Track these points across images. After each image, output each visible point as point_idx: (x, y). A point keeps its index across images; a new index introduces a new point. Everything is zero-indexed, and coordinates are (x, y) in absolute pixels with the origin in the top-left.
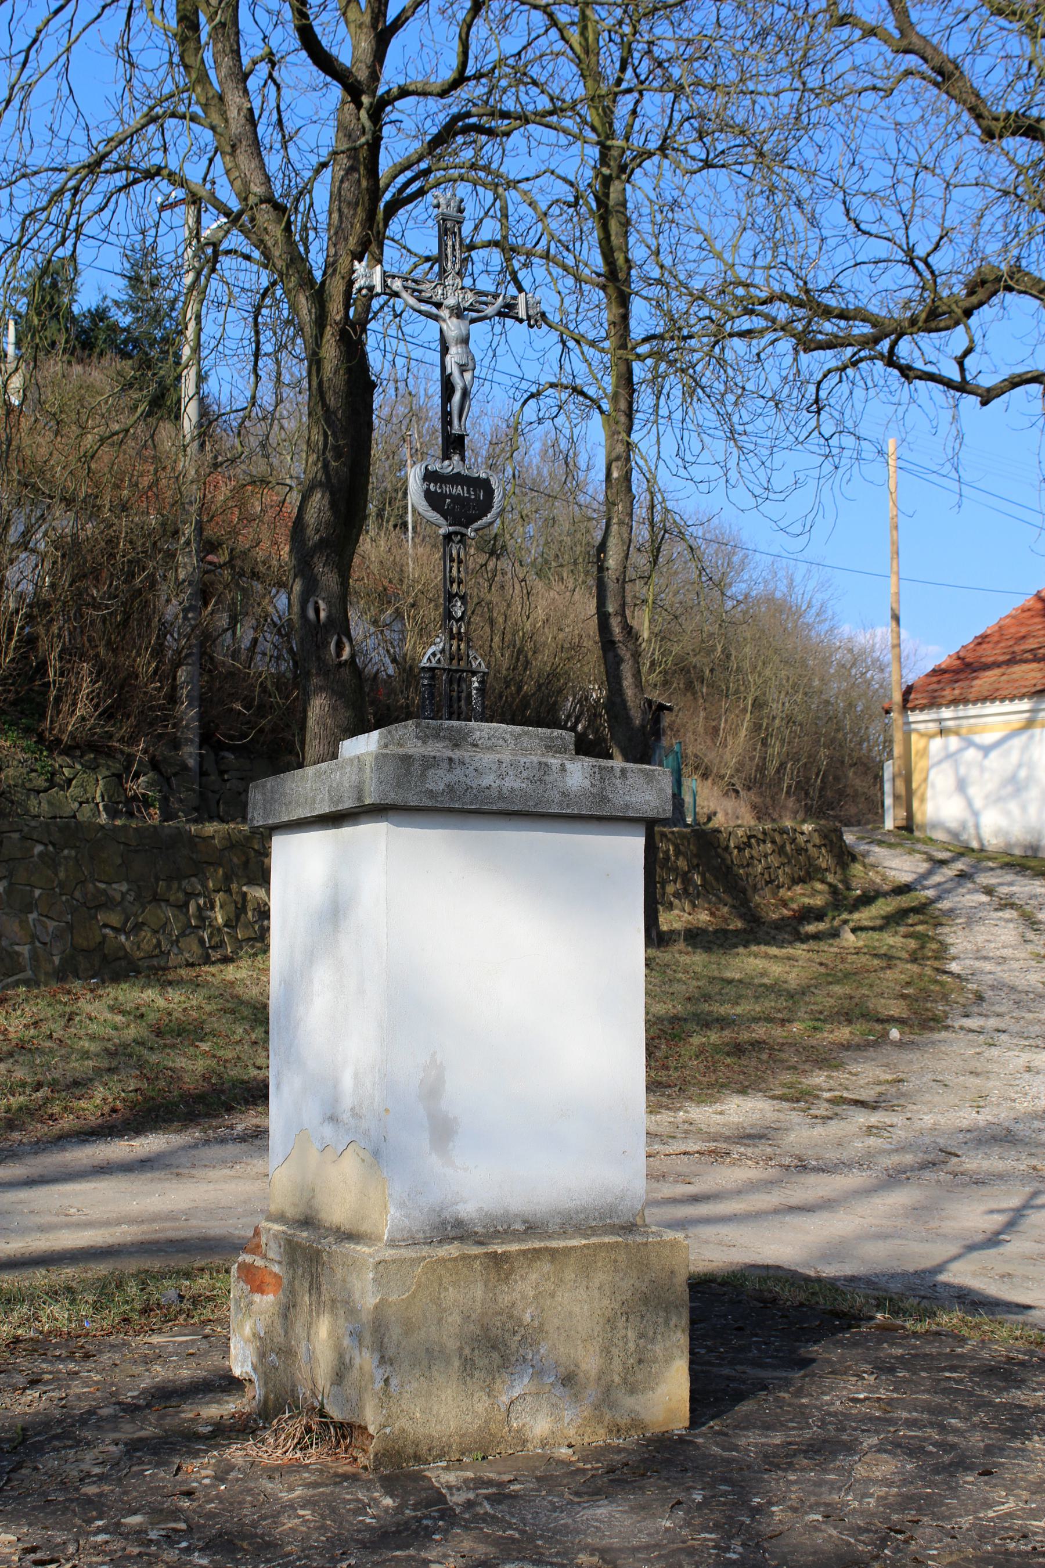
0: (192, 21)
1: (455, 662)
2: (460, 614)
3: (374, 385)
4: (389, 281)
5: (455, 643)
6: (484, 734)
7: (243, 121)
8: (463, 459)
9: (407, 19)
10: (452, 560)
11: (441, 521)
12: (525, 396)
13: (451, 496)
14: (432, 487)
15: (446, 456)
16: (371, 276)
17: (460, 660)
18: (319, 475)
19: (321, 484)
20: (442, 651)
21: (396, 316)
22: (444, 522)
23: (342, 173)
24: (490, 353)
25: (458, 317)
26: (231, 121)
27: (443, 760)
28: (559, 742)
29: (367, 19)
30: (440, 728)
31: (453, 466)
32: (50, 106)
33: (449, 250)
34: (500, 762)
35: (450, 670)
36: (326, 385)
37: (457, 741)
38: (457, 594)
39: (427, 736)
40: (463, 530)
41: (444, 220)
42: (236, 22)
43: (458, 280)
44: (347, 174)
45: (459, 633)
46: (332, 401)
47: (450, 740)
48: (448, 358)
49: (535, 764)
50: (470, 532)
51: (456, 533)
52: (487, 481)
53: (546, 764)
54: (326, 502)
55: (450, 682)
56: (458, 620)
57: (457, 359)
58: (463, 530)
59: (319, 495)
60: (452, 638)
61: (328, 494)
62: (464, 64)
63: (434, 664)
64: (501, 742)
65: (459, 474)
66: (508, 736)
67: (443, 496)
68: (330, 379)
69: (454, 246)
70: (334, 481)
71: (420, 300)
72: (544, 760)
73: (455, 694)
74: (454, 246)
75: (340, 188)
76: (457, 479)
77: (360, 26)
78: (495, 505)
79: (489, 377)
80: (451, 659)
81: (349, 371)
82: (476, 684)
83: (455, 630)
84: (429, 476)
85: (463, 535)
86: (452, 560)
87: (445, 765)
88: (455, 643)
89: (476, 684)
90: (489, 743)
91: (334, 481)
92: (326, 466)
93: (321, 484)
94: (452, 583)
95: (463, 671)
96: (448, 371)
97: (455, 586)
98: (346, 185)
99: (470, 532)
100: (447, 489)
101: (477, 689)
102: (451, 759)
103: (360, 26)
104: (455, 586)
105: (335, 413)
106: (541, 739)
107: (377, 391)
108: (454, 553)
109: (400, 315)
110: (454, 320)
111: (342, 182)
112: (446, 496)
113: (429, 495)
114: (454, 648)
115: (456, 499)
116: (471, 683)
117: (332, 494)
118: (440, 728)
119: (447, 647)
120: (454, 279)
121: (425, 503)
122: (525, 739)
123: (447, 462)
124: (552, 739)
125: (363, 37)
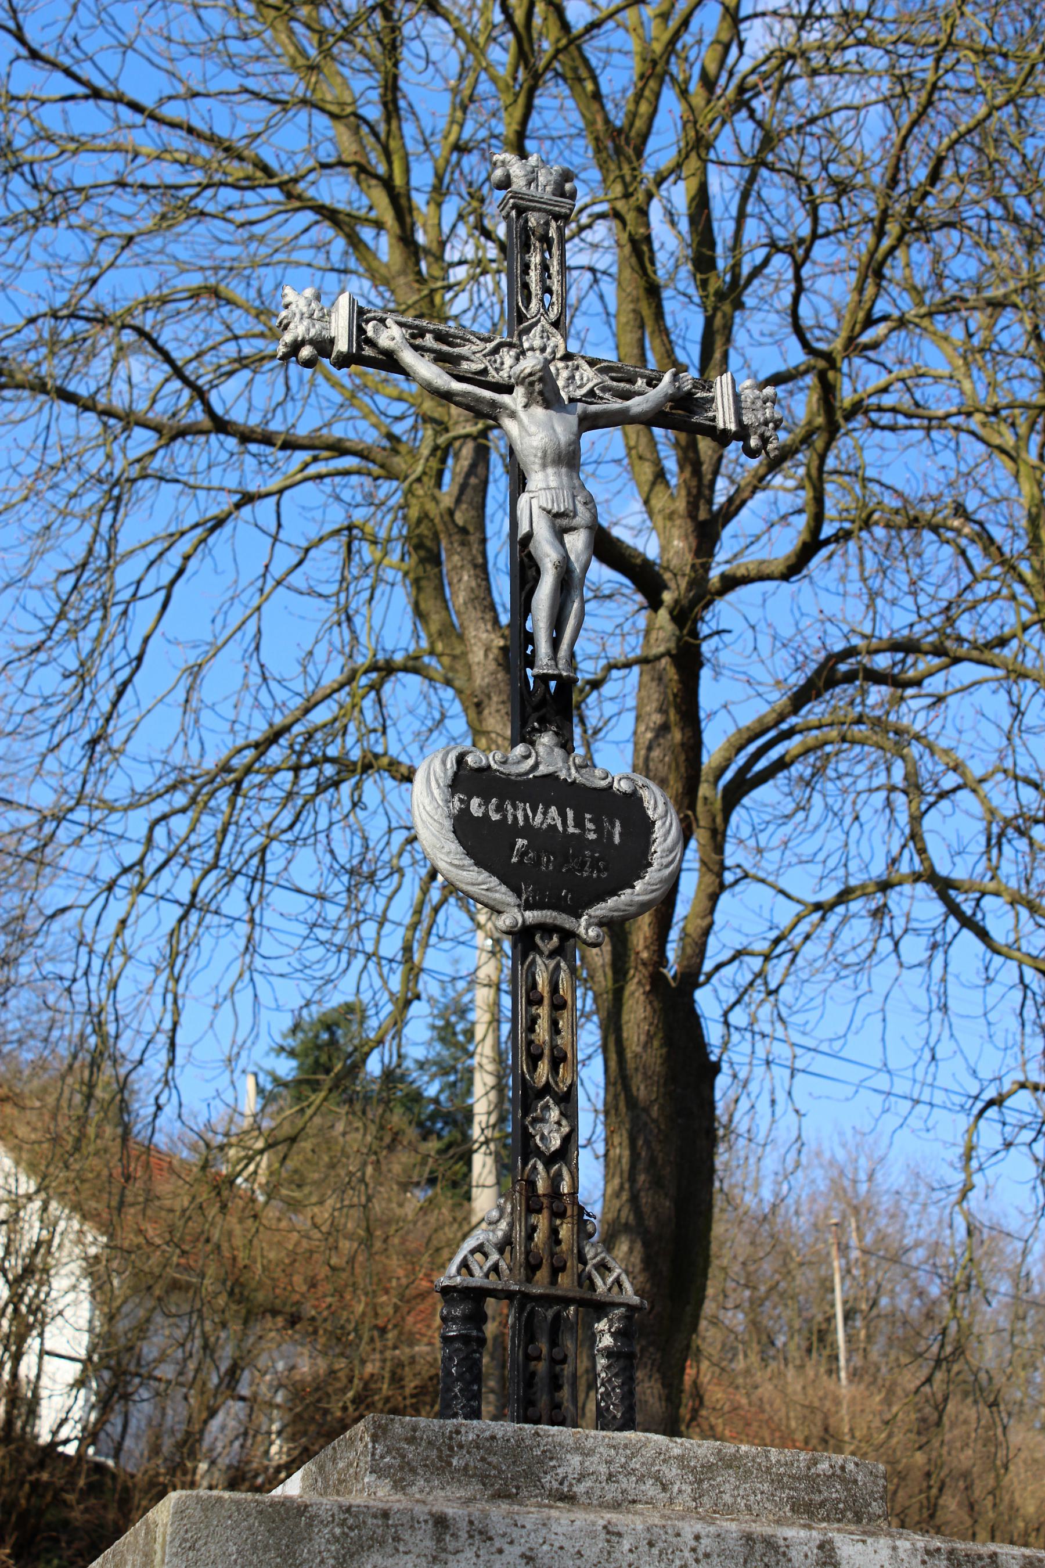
0: (429, 550)
1: (542, 1275)
2: (556, 1143)
3: (715, 1069)
4: (370, 328)
5: (542, 1221)
6: (594, 1463)
7: (492, 666)
8: (567, 746)
9: (743, 503)
10: (534, 1001)
11: (503, 894)
12: (980, 1105)
13: (527, 831)
14: (476, 807)
15: (523, 735)
16: (325, 317)
17: (556, 1271)
18: (624, 1214)
19: (627, 1228)
20: (505, 1245)
21: (770, 993)
22: (511, 898)
23: (649, 735)
24: (927, 1055)
25: (547, 405)
26: (475, 668)
27: (413, 1523)
28: (836, 1492)
29: (681, 505)
30: (451, 1444)
31: (544, 756)
32: (233, 700)
33: (534, 276)
34: (612, 1533)
35: (526, 1297)
36: (631, 1065)
37: (514, 1478)
38: (547, 1089)
39: (409, 1468)
40: (565, 921)
41: (521, 211)
42: (482, 527)
43: (557, 339)
44: (657, 736)
45: (555, 1193)
46: (642, 1090)
47: (484, 1479)
48: (524, 499)
49: (732, 1543)
50: (585, 927)
51: (547, 929)
52: (633, 799)
53: (769, 1543)
54: (636, 1259)
55: (528, 1331)
56: (550, 1160)
57: (544, 500)
58: (565, 921)
59: (625, 1248)
60: (532, 1207)
61: (638, 1246)
62: (818, 519)
63: (478, 1279)
64: (649, 1488)
65: (552, 777)
66: (671, 1472)
67: (509, 831)
68: (636, 1056)
69: (545, 267)
70: (650, 1223)
71: (460, 379)
72: (760, 1529)
73: (541, 1367)
74: (545, 267)
75: (647, 759)
76: (545, 789)
77: (671, 517)
78: (656, 861)
79: (925, 1097)
80: (532, 1267)
81: (669, 1041)
82: (607, 1341)
83: (541, 1186)
84: (466, 780)
85: (568, 935)
86: (534, 1001)
87: (423, 1540)
88: (542, 1221)
89: (607, 1341)
90: (611, 1492)
91: (650, 1223)
92: (634, 1199)
93: (627, 1228)
94: (534, 1060)
95: (566, 1301)
96: (524, 529)
97: (543, 1068)
98: (656, 753)
99: (585, 927)
100: (519, 813)
101: (609, 1353)
102: (441, 1522)
103: (671, 517)
104: (543, 1068)
105: (646, 1110)
106: (778, 1482)
107: (722, 1081)
108: (542, 980)
109: (776, 991)
110: (538, 411)
111: (650, 748)
112: (516, 831)
113: (465, 829)
114: (539, 1237)
115: (544, 840)
116: (592, 1338)
117: (646, 1245)
118: (451, 1444)
119: (519, 1235)
120: (545, 335)
121: (453, 846)
122: (728, 1482)
123: (520, 749)
124: (813, 1482)
125: (676, 532)
